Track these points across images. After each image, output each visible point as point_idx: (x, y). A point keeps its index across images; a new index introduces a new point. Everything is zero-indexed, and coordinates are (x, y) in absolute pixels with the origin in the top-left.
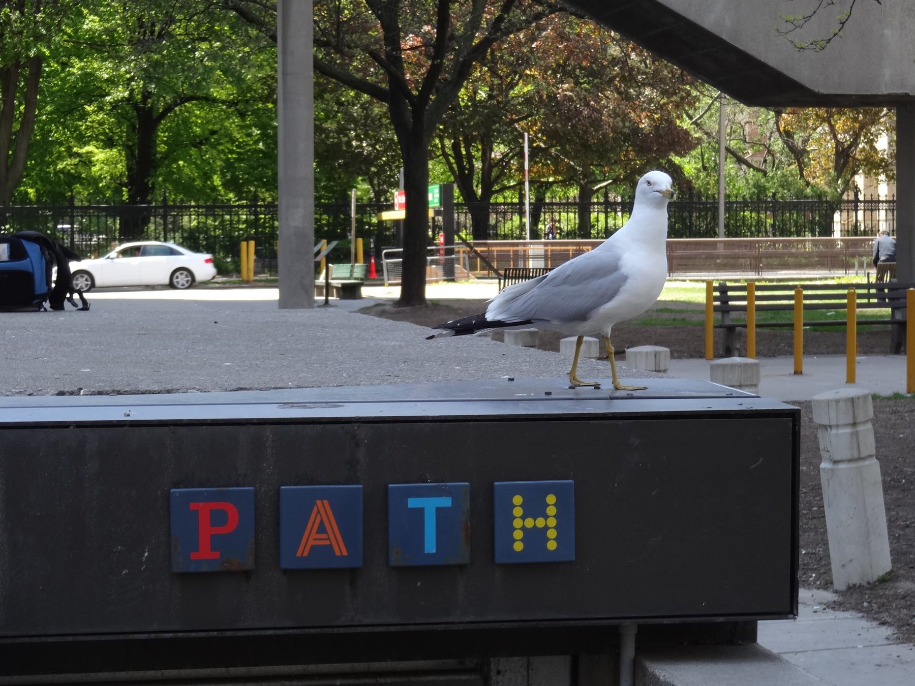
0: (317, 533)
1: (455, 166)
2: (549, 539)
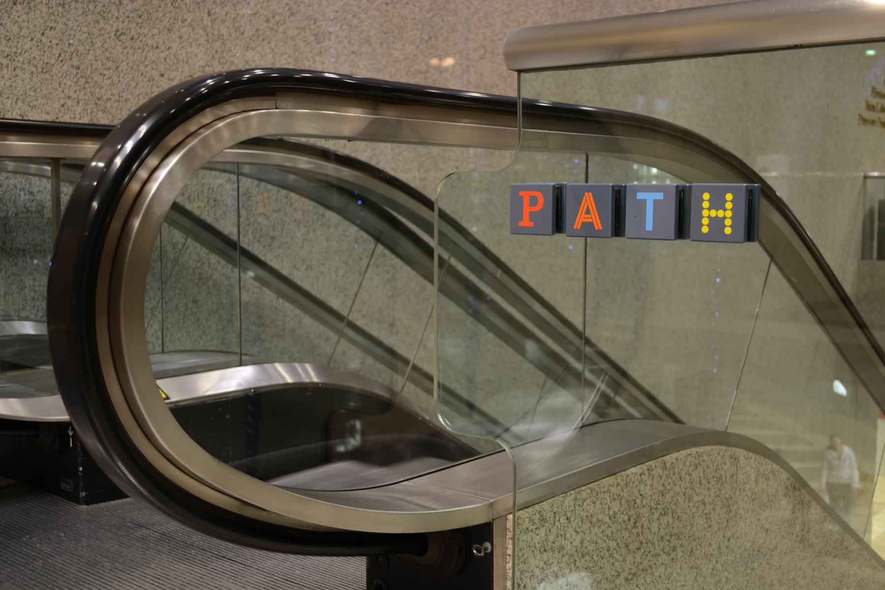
0: (586, 214)
2: (730, 226)
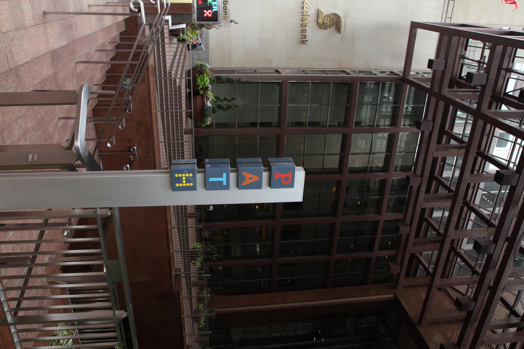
0: (249, 178)
1: (415, 160)
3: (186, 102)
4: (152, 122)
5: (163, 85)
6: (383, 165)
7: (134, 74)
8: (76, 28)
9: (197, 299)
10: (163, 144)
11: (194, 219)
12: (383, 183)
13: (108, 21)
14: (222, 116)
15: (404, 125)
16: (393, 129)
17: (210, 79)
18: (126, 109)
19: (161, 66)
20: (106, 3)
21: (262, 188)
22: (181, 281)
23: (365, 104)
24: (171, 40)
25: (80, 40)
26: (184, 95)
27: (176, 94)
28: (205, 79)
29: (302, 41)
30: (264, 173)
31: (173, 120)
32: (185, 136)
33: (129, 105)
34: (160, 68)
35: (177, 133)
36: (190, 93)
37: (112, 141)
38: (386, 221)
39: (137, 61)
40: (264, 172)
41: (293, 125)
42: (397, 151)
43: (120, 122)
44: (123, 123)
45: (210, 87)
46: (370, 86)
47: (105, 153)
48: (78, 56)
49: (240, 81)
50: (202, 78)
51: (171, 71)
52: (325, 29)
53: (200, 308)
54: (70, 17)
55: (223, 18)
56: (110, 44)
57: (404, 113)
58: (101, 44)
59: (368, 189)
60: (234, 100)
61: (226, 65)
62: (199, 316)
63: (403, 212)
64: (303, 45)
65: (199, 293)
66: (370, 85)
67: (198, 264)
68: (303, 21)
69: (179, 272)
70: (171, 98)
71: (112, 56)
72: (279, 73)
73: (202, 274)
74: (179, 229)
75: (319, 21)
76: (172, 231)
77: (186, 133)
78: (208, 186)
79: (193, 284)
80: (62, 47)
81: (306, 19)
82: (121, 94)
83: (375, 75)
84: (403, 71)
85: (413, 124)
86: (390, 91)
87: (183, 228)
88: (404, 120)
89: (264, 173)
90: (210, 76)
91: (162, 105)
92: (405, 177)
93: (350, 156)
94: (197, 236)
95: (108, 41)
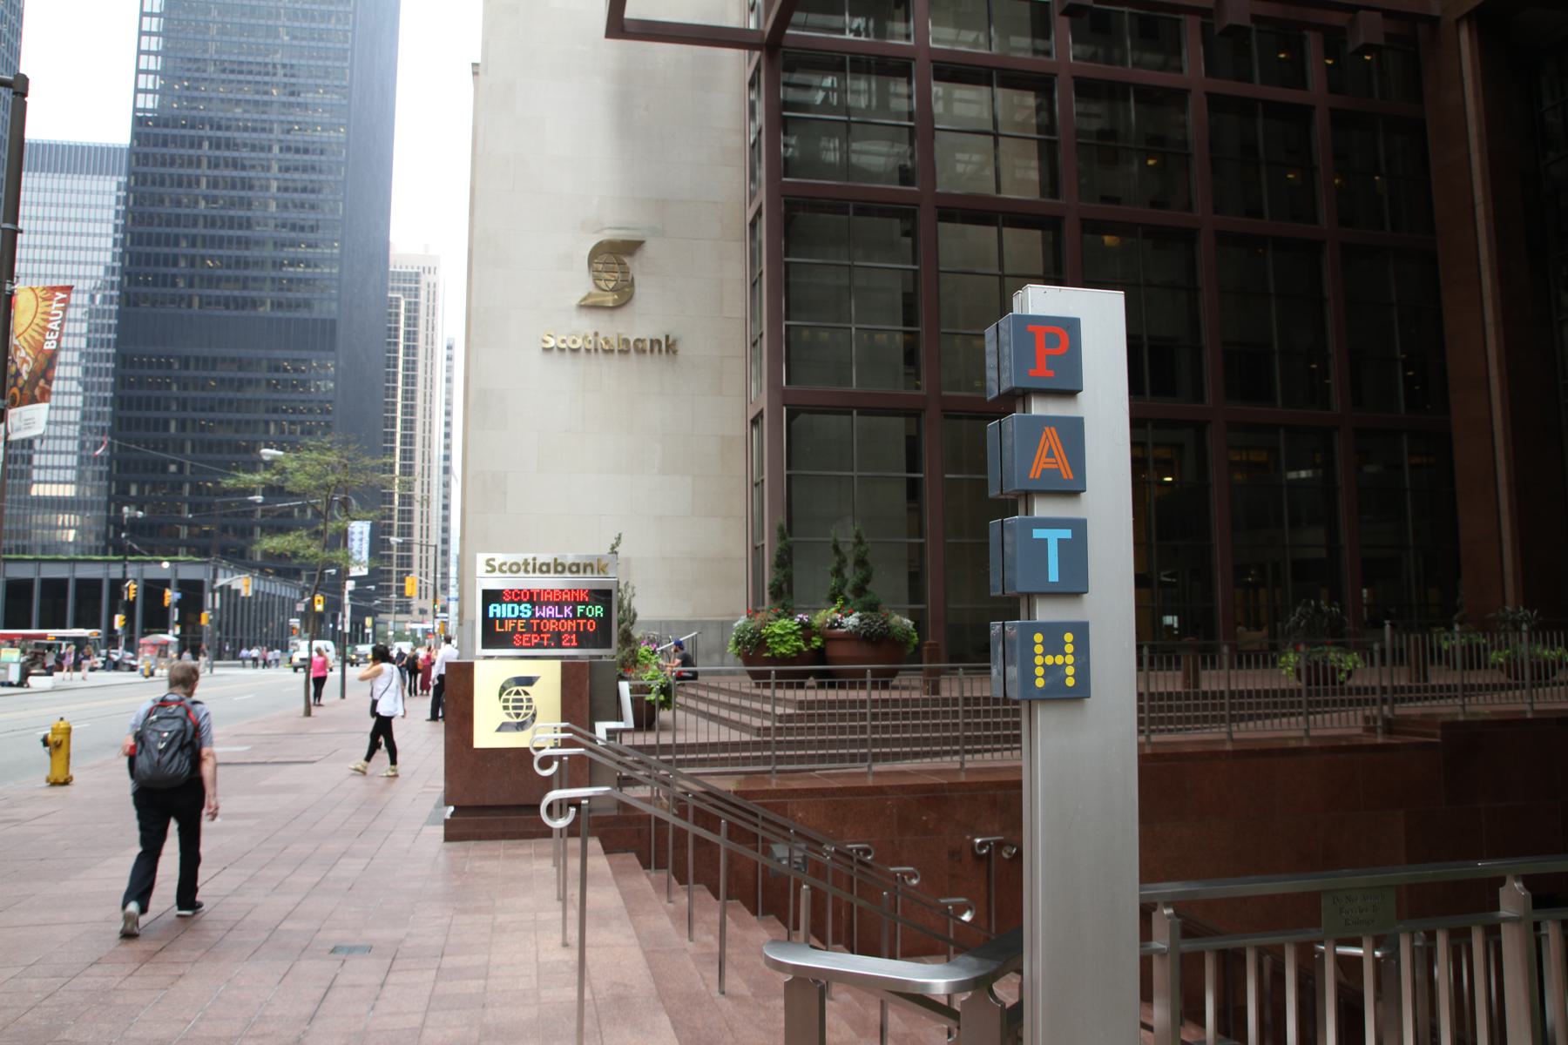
3: (842, 686)
4: (902, 788)
5: (792, 753)
6: (1033, 93)
7: (761, 833)
8: (625, 986)
9: (1472, 668)
10: (968, 757)
11: (1204, 674)
12: (1086, 88)
13: (604, 896)
14: (889, 583)
15: (908, 37)
16: (920, 68)
17: (779, 616)
18: (860, 862)
19: (737, 758)
20: (559, 899)
21: (1082, 419)
22: (1409, 716)
23: (848, 158)
24: (664, 728)
25: (657, 977)
26: (822, 695)
27: (819, 715)
28: (778, 631)
29: (667, 351)
30: (1034, 412)
31: (898, 726)
32: (945, 694)
33: (849, 853)
34: (745, 761)
35: (935, 715)
36: (818, 674)
37: (955, 906)
38: (1210, 71)
39: (720, 819)
40: (1030, 412)
41: (913, 371)
42: (988, 52)
43: (899, 880)
44: (903, 873)
45: (800, 616)
46: (792, 146)
47: (993, 931)
48: (704, 988)
49: (785, 528)
50: (777, 639)
51: (753, 728)
52: (632, 284)
53: (1501, 660)
54: (594, 999)
55: (602, 575)
56: (674, 898)
57: (872, 39)
58: (673, 923)
59: (1106, 135)
60: (840, 548)
61: (740, 570)
62: (1532, 666)
63: (1180, 20)
64: (680, 348)
65: (1447, 663)
66: (791, 146)
67: (1351, 660)
68: (611, 351)
69: (1375, 722)
70: (832, 730)
71: (708, 894)
72: (762, 417)
73: (1383, 651)
74: (1233, 719)
75: (611, 305)
76: (1240, 740)
77: (936, 690)
78: (1074, 587)
79: (1418, 680)
80: (675, 1029)
81: (607, 342)
82: (818, 870)
83: (759, 133)
84: (747, 51)
85: (903, 8)
86: (807, 87)
87: (1232, 706)
88: (893, 36)
89: (1034, 412)
90: (771, 617)
91: (853, 758)
92: (1066, 20)
93: (1005, 195)
94: (1257, 666)
95: (665, 902)
